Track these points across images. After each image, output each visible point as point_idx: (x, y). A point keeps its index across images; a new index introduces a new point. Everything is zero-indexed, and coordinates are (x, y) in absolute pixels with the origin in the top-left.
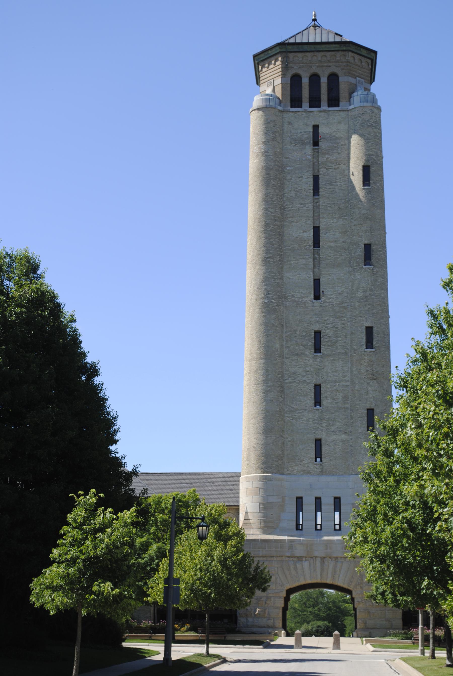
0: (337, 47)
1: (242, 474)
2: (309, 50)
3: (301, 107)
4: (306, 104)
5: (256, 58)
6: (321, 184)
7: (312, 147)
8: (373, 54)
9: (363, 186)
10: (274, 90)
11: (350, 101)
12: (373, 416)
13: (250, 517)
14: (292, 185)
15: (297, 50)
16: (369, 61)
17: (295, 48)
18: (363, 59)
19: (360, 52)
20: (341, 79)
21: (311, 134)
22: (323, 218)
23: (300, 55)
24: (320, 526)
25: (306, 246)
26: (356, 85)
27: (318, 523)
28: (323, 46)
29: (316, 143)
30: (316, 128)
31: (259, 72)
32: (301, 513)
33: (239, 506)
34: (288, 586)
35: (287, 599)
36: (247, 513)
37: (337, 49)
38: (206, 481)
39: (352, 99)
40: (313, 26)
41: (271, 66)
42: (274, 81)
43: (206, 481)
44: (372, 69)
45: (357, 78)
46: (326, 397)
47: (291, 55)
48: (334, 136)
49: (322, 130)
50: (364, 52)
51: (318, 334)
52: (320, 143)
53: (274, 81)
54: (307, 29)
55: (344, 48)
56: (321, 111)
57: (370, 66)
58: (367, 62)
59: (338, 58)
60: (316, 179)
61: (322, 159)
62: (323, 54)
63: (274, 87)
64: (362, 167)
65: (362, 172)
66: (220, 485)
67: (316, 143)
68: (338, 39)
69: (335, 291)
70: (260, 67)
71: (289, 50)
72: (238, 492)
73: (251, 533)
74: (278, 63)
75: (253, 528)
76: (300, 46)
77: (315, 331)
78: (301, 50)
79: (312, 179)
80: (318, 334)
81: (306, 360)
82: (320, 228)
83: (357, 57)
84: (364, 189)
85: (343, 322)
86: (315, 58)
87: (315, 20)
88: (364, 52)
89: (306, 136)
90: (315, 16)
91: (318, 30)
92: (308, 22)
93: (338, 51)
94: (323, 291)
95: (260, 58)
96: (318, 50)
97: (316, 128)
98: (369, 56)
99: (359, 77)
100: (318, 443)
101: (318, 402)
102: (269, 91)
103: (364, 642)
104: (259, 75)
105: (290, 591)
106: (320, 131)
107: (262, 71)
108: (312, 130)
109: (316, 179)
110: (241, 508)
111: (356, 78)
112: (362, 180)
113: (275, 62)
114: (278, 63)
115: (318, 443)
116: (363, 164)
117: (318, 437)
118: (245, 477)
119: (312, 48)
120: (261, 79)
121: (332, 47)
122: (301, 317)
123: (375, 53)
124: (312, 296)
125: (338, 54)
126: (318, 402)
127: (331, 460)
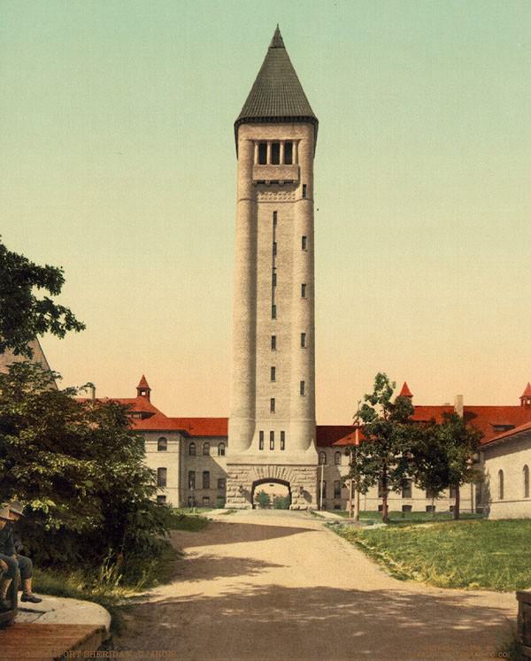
30: (275, 213)
124: (286, 433)
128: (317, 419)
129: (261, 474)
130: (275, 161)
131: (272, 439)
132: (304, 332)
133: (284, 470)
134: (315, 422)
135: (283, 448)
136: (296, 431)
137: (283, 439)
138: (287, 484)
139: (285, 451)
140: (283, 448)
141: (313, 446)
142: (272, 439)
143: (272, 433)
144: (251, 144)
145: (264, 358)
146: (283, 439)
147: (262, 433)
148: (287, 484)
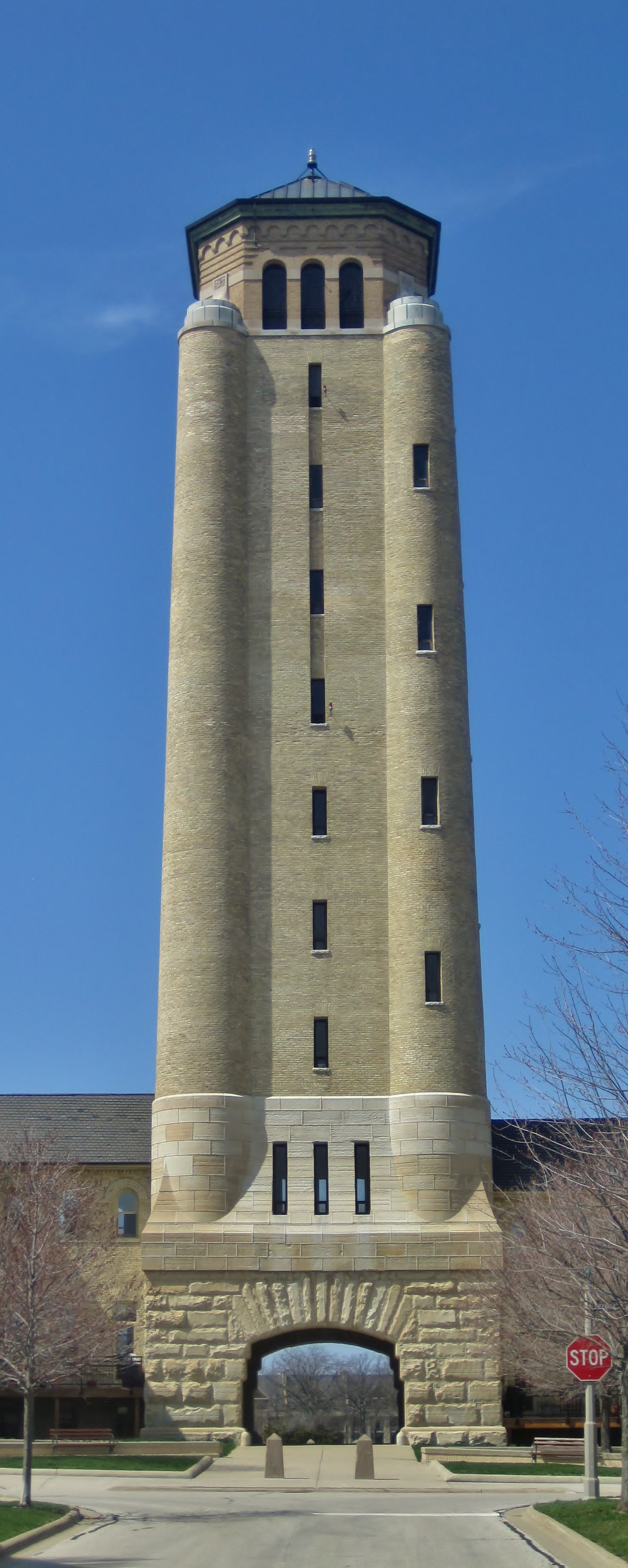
0: (358, 209)
1: (156, 1096)
2: (300, 214)
3: (284, 326)
4: (294, 324)
5: (193, 233)
6: (327, 482)
7: (307, 407)
8: (432, 229)
9: (415, 486)
10: (228, 294)
11: (385, 316)
12: (426, 459)
13: (174, 1187)
14: (265, 485)
15: (277, 214)
16: (425, 242)
17: (273, 211)
18: (413, 238)
19: (405, 222)
20: (366, 274)
21: (306, 382)
22: (331, 552)
23: (283, 225)
24: (324, 1205)
25: (295, 610)
26: (397, 285)
27: (321, 1200)
28: (330, 207)
29: (315, 400)
30: (315, 369)
31: (198, 262)
32: (284, 1181)
33: (150, 1164)
34: (254, 1331)
35: (253, 1365)
36: (166, 1178)
37: (358, 213)
38: (81, 1110)
39: (390, 313)
40: (309, 177)
41: (223, 247)
42: (228, 276)
43: (81, 1110)
44: (429, 258)
45: (401, 273)
46: (339, 929)
47: (264, 226)
48: (354, 387)
49: (325, 373)
50: (413, 223)
51: (319, 795)
52: (324, 400)
53: (228, 276)
54: (298, 181)
55: (374, 212)
56: (325, 337)
57: (427, 252)
58: (421, 244)
59: (361, 232)
60: (316, 474)
61: (329, 430)
62: (329, 222)
63: (228, 288)
64: (411, 447)
65: (411, 459)
66: (111, 1119)
67: (315, 400)
68: (358, 195)
69: (357, 705)
70: (201, 251)
71: (261, 215)
72: (148, 1134)
73: (176, 1221)
74: (237, 239)
75: (178, 1209)
76: (282, 207)
77: (314, 787)
78: (285, 214)
79: (307, 474)
80: (319, 795)
81: (295, 848)
82: (325, 574)
83: (399, 231)
84: (424, 830)
85: (373, 769)
86: (313, 231)
87: (312, 166)
88: (413, 223)
89: (294, 385)
90: (314, 157)
91: (319, 182)
92: (301, 169)
93: (360, 217)
94: (331, 705)
95: (201, 233)
96: (318, 214)
97: (315, 369)
98: (424, 231)
99: (403, 270)
100: (321, 1025)
101: (320, 939)
102: (220, 295)
103: (424, 1456)
104: (198, 269)
105: (260, 1348)
106: (323, 376)
107: (203, 258)
108: (307, 375)
109: (316, 474)
110: (154, 1167)
111: (397, 272)
112: (423, 988)
113: (232, 237)
114: (237, 239)
115: (321, 1025)
116: (414, 442)
117: (321, 1014)
118: (162, 1100)
119: (308, 210)
120: (202, 274)
121: (348, 209)
122: (285, 759)
123: (437, 225)
124: (308, 715)
125: (361, 224)
126: (320, 939)
127: (348, 1064)
128: (492, 1093)
129: (282, 1312)
130: (313, 317)
131: (321, 1171)
132: (430, 774)
133: (371, 1292)
134: (486, 1106)
135: (363, 1206)
136: (406, 1114)
137: (362, 1169)
138: (384, 1346)
139: (310, 360)
140: (363, 1206)
141: (480, 1196)
142: (321, 1171)
143: (321, 1151)
144: (426, 1397)
145: (294, 868)
146: (362, 1169)
147: (280, 1149)
148: (384, 1346)
